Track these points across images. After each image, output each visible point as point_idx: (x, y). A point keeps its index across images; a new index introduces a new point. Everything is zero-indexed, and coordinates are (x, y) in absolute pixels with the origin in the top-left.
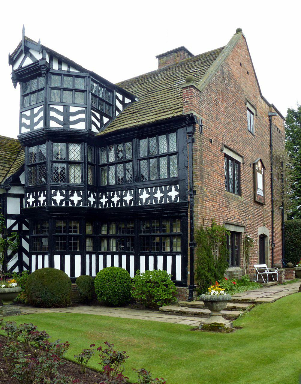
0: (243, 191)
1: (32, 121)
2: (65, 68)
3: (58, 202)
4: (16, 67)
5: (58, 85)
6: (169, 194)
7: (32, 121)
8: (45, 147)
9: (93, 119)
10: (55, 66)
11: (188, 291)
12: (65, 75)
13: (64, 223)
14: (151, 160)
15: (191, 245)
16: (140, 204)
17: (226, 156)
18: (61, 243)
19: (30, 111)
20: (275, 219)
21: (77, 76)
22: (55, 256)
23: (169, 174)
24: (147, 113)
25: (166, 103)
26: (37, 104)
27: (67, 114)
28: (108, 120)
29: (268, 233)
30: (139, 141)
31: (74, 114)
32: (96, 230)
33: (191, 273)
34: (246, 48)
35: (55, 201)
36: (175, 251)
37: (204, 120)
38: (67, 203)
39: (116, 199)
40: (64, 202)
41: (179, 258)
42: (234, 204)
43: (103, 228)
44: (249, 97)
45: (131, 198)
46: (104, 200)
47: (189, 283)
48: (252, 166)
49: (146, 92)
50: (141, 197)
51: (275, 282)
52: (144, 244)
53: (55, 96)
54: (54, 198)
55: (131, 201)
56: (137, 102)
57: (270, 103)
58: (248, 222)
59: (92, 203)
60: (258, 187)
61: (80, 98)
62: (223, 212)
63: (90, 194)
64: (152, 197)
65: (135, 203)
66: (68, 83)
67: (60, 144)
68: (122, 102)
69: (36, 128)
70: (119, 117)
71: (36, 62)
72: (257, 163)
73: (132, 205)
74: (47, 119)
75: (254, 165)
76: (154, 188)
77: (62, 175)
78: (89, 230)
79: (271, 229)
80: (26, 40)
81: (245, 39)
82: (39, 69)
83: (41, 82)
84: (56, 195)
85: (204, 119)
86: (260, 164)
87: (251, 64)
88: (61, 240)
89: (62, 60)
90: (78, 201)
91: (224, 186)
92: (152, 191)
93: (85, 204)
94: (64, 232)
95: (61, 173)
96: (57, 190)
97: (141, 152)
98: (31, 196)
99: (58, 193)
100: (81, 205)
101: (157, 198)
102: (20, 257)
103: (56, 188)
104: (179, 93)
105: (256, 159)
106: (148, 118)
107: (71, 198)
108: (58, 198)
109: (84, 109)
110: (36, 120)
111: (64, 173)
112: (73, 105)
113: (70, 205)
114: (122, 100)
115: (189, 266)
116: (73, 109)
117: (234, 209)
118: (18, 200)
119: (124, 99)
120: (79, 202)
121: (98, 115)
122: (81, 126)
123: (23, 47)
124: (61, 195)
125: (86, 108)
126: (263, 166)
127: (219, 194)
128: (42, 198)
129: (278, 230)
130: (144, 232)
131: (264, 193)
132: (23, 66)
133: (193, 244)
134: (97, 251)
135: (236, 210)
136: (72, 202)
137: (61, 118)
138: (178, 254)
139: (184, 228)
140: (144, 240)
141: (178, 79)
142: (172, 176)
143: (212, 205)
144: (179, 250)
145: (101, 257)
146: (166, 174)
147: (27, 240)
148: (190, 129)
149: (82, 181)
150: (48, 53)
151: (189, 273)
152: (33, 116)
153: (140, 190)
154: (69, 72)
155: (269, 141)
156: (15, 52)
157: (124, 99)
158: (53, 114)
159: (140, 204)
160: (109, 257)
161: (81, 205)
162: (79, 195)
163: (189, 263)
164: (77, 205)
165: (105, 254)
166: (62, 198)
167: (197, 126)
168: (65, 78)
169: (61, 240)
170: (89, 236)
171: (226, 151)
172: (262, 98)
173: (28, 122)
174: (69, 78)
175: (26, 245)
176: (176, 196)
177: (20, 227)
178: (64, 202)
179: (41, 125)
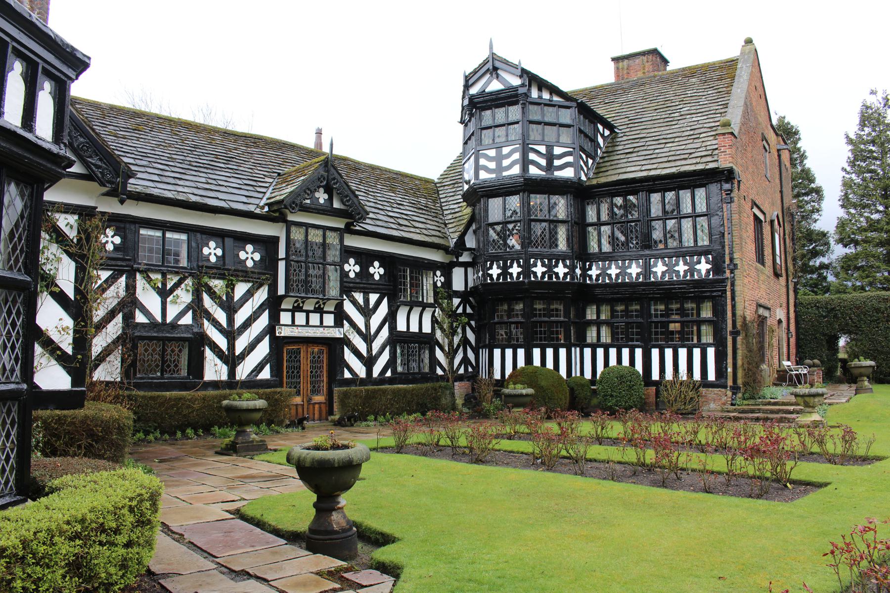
1: (499, 164)
2: (546, 96)
7: (499, 164)
8: (518, 200)
10: (535, 94)
12: (546, 105)
13: (544, 304)
17: (755, 215)
18: (541, 331)
19: (494, 150)
21: (560, 107)
22: (534, 349)
26: (508, 143)
27: (550, 157)
30: (649, 196)
35: (535, 274)
36: (704, 340)
38: (550, 277)
39: (594, 272)
40: (547, 276)
41: (711, 352)
43: (588, 312)
47: (730, 383)
50: (654, 270)
52: (656, 333)
53: (535, 132)
54: (534, 269)
61: (566, 136)
64: (670, 270)
65: (645, 277)
66: (550, 115)
67: (538, 196)
69: (505, 174)
76: (674, 259)
77: (543, 239)
80: (493, 57)
82: (516, 96)
83: (515, 112)
84: (536, 266)
89: (543, 84)
90: (631, 268)
92: (670, 262)
93: (572, 278)
94: (545, 316)
95: (541, 235)
96: (537, 259)
97: (653, 211)
100: (568, 280)
101: (678, 272)
102: (370, 349)
103: (536, 256)
107: (556, 270)
108: (539, 270)
109: (572, 150)
110: (506, 163)
111: (545, 236)
112: (558, 144)
113: (554, 280)
116: (557, 151)
121: (584, 156)
122: (568, 173)
125: (574, 148)
130: (656, 316)
132: (487, 90)
133: (735, 333)
136: (557, 274)
138: (710, 345)
139: (720, 311)
140: (656, 327)
142: (700, 243)
144: (710, 340)
145: (588, 352)
146: (692, 241)
148: (727, 186)
149: (568, 246)
150: (528, 77)
152: (499, 158)
153: (652, 260)
155: (779, 186)
156: (475, 72)
158: (532, 156)
160: (600, 352)
161: (568, 280)
162: (565, 266)
164: (563, 279)
166: (545, 269)
167: (736, 182)
168: (546, 108)
173: (492, 165)
174: (551, 109)
175: (471, 336)
177: (464, 309)
178: (547, 276)
179: (516, 170)
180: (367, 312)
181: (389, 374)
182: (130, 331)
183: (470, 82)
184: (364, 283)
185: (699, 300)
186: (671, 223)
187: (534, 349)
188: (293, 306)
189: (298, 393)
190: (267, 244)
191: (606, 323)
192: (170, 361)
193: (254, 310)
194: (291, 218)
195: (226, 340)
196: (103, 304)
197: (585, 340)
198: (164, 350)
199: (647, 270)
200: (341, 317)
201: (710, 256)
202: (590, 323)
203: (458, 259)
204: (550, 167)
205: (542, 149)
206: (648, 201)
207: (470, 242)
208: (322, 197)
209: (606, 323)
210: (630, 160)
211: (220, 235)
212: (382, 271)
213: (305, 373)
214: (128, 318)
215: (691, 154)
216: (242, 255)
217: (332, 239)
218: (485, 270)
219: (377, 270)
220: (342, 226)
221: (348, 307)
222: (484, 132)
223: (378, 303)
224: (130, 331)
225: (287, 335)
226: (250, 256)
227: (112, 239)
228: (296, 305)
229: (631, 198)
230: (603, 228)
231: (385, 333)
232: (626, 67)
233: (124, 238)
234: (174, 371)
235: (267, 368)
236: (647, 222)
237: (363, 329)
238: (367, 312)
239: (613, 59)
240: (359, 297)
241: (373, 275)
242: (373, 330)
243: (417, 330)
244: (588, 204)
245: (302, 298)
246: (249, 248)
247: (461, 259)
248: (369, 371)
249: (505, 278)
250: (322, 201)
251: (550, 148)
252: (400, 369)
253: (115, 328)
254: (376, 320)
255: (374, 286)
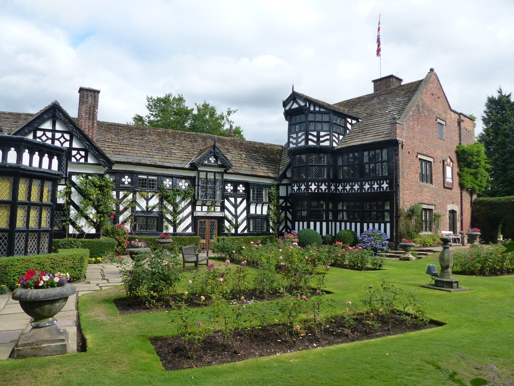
0: (434, 181)
1: (297, 141)
2: (317, 109)
3: (313, 190)
4: (287, 108)
5: (313, 119)
6: (382, 186)
7: (297, 141)
9: (334, 138)
10: (312, 109)
11: (394, 245)
14: (371, 165)
15: (396, 217)
16: (364, 191)
17: (420, 159)
18: (314, 214)
20: (464, 198)
22: (323, 223)
23: (382, 174)
24: (368, 134)
25: (380, 127)
26: (300, 131)
27: (318, 137)
28: (342, 137)
29: (457, 208)
31: (323, 136)
32: (335, 206)
33: (396, 234)
34: (437, 81)
35: (311, 189)
37: (404, 140)
38: (318, 190)
39: (348, 188)
41: (388, 225)
42: (426, 190)
44: (439, 114)
45: (358, 187)
46: (340, 188)
48: (442, 162)
49: (366, 114)
50: (364, 187)
51: (458, 244)
54: (311, 187)
55: (358, 189)
56: (360, 123)
57: (459, 112)
58: (438, 201)
59: (333, 190)
60: (447, 177)
62: (418, 196)
63: (332, 184)
66: (318, 118)
68: (351, 124)
69: (299, 145)
70: (349, 134)
71: (300, 107)
72: (447, 160)
73: (359, 192)
74: (307, 140)
75: (443, 161)
78: (331, 206)
79: (460, 206)
81: (436, 75)
83: (303, 118)
85: (404, 140)
86: (449, 160)
87: (441, 90)
88: (314, 213)
90: (325, 189)
91: (419, 180)
93: (329, 191)
97: (365, 159)
98: (296, 186)
99: (313, 184)
102: (236, 221)
104: (389, 119)
105: (446, 156)
106: (370, 138)
107: (321, 187)
110: (300, 140)
113: (320, 191)
114: (350, 122)
115: (395, 229)
116: (322, 134)
117: (426, 194)
118: (285, 187)
119: (352, 121)
120: (325, 189)
121: (337, 135)
122: (327, 143)
123: (292, 97)
124: (315, 185)
126: (452, 161)
127: (414, 185)
128: (303, 187)
129: (467, 206)
131: (452, 180)
134: (335, 219)
135: (428, 194)
136: (321, 189)
137: (315, 139)
138: (388, 222)
141: (388, 106)
143: (410, 192)
144: (388, 220)
145: (338, 224)
147: (290, 212)
151: (395, 234)
152: (297, 138)
154: (320, 111)
156: (287, 100)
157: (352, 121)
158: (310, 137)
159: (364, 191)
160: (343, 224)
161: (327, 192)
162: (325, 185)
163: (395, 228)
165: (341, 222)
166: (316, 187)
169: (314, 213)
170: (331, 210)
171: (420, 156)
172: (452, 110)
173: (294, 141)
174: (320, 115)
175: (289, 216)
176: (386, 187)
177: (286, 204)
179: (303, 143)
180: (236, 206)
181: (246, 232)
182: (133, 214)
183: (286, 104)
184: (235, 193)
185: (384, 201)
186: (372, 165)
187: (323, 223)
188: (202, 204)
189: (204, 238)
190: (192, 180)
191: (345, 211)
192: (150, 225)
193: (185, 205)
194: (199, 169)
195: (288, 216)
196: (273, 190)
197: (338, 218)
198: (147, 221)
199: (361, 187)
200: (223, 208)
201: (388, 181)
202: (340, 211)
203: (281, 183)
204: (318, 141)
205: (315, 133)
206: (363, 156)
207: (289, 175)
208: (212, 160)
209: (345, 211)
210: (359, 135)
211: (171, 177)
212: (244, 189)
213: (207, 230)
214: (133, 208)
215: (383, 132)
216: (180, 184)
217: (218, 177)
218: (292, 187)
219: (241, 188)
220: (223, 171)
221: (227, 204)
222: (312, 123)
223: (241, 202)
224: (133, 214)
225: (198, 215)
226: (183, 184)
227: (127, 180)
228: (203, 203)
229: (356, 154)
230: (384, 164)
231: (245, 214)
232: (378, 85)
233: (132, 179)
234: (151, 229)
235: (190, 228)
236: (362, 166)
237: (234, 213)
238: (236, 206)
239: (373, 81)
240: (232, 200)
241: (239, 191)
242: (238, 214)
243: (254, 213)
244: (339, 157)
245: (205, 201)
246: (183, 181)
247: (282, 183)
248: (236, 231)
249: (299, 191)
250: (212, 162)
251: (318, 133)
252: (251, 230)
253: (127, 213)
254: (240, 210)
255: (239, 195)
